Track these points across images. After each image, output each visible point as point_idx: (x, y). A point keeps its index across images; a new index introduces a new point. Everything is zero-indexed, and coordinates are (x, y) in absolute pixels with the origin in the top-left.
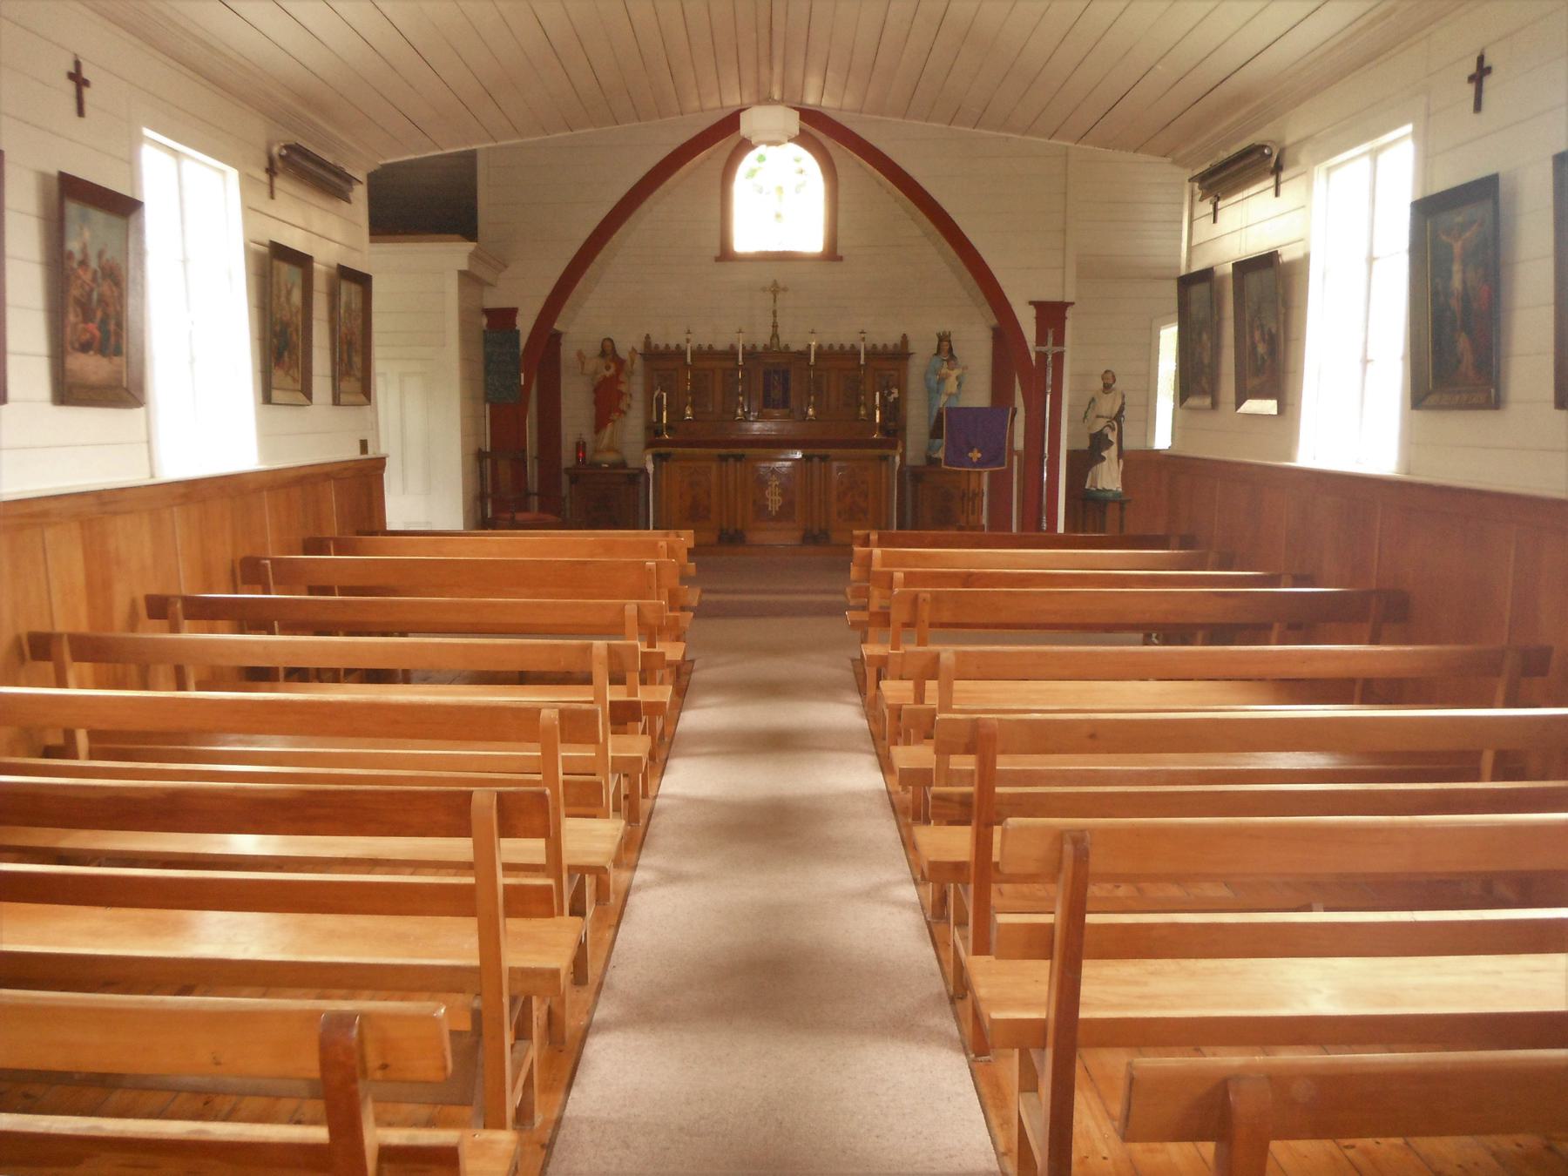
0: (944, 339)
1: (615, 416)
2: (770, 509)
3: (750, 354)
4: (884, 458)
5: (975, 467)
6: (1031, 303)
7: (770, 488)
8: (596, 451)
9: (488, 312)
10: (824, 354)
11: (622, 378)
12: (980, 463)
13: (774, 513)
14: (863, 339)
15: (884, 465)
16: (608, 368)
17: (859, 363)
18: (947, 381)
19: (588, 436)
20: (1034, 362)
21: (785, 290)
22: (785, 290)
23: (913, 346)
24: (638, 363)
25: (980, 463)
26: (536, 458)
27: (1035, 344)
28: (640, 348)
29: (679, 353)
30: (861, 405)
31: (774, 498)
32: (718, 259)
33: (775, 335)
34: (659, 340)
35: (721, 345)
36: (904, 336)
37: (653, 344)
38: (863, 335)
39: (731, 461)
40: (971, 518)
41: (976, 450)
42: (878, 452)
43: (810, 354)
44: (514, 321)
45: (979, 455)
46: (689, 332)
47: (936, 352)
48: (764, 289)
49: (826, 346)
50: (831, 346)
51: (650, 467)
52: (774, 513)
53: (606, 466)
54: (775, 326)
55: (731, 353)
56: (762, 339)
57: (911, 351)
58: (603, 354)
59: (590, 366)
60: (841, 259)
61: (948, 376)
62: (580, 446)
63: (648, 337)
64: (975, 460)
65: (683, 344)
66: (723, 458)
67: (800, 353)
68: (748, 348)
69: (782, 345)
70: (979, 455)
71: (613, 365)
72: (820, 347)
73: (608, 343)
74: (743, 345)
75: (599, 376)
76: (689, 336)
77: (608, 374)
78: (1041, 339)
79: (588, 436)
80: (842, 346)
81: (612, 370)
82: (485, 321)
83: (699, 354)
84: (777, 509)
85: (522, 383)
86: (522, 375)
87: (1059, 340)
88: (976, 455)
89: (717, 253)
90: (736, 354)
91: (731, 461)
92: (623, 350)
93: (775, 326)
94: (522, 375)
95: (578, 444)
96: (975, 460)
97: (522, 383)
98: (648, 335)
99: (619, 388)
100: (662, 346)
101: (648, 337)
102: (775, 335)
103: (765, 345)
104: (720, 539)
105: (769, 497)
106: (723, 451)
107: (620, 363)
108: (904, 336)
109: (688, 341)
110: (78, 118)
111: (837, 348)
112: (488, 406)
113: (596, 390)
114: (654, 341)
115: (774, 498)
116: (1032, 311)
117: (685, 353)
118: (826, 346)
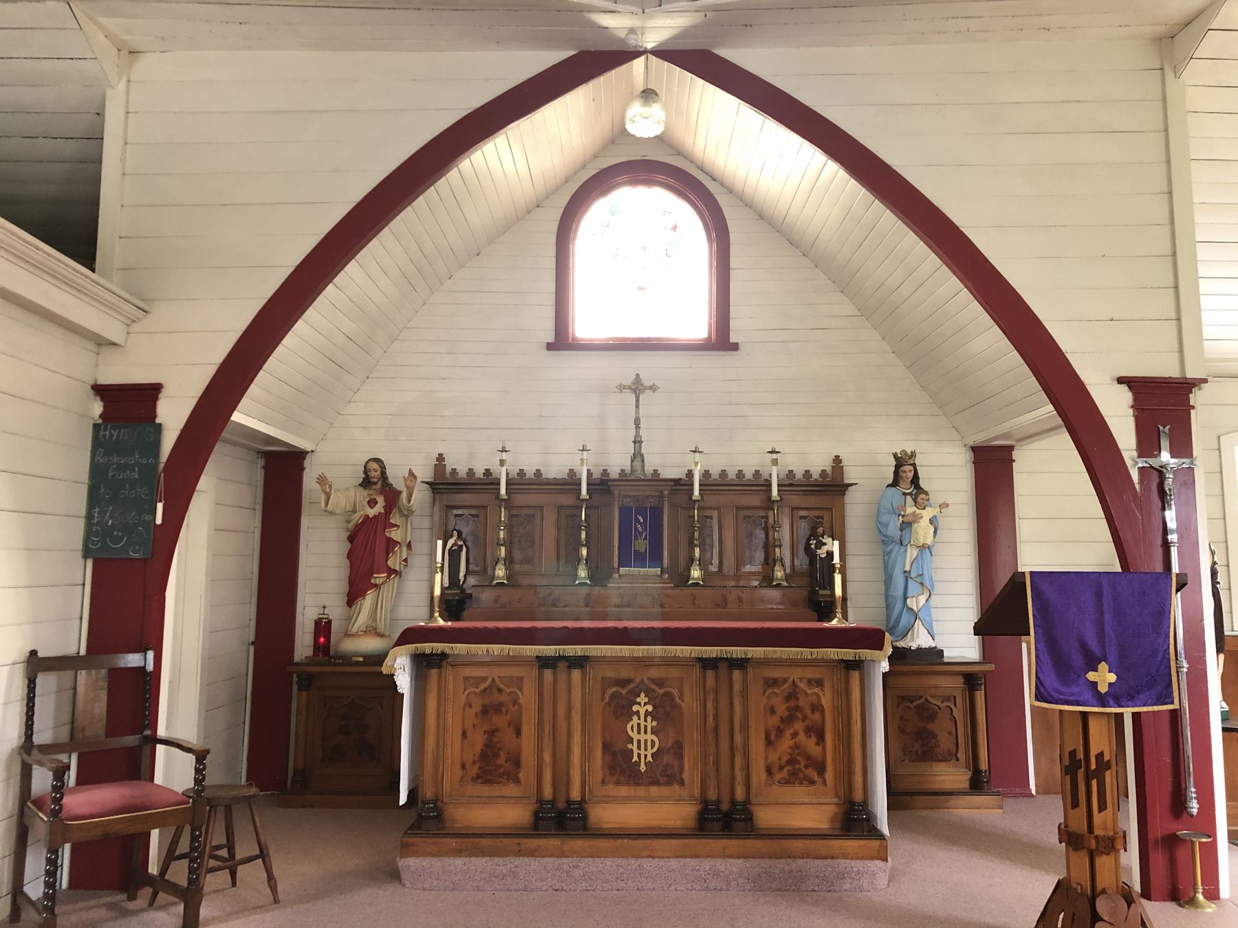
0: (901, 461)
1: (379, 578)
2: (635, 758)
3: (602, 485)
4: (856, 665)
5: (1103, 704)
6: (1121, 380)
7: (635, 718)
8: (347, 635)
9: (101, 390)
10: (715, 485)
11: (395, 518)
12: (1116, 695)
13: (643, 768)
14: (775, 462)
15: (855, 675)
16: (372, 503)
17: (770, 497)
18: (915, 526)
19: (336, 612)
20: (1137, 486)
21: (653, 388)
22: (653, 388)
23: (850, 475)
24: (421, 496)
25: (1116, 695)
26: (253, 643)
27: (1135, 454)
28: (425, 472)
29: (489, 481)
30: (774, 562)
31: (642, 737)
32: (550, 347)
33: (638, 456)
34: (459, 462)
35: (555, 469)
36: (837, 460)
37: (448, 470)
38: (774, 456)
39: (562, 665)
40: (1097, 818)
41: (1103, 666)
42: (848, 654)
43: (692, 485)
44: (154, 407)
45: (1112, 678)
46: (503, 450)
47: (890, 481)
48: (621, 388)
49: (715, 473)
50: (723, 473)
51: (404, 682)
52: (643, 768)
53: (361, 659)
54: (637, 442)
55: (572, 482)
56: (618, 461)
57: (846, 481)
58: (366, 483)
59: (340, 501)
60: (735, 347)
61: (916, 518)
62: (323, 627)
63: (441, 458)
64: (1103, 689)
65: (494, 465)
66: (545, 663)
67: (677, 482)
68: (597, 475)
69: (649, 470)
70: (1112, 678)
71: (381, 500)
72: (706, 474)
73: (375, 466)
74: (589, 471)
75: (357, 515)
76: (505, 456)
77: (372, 512)
78: (1147, 445)
79: (336, 612)
80: (740, 474)
81: (379, 508)
82: (97, 408)
83: (518, 483)
84: (649, 758)
85: (159, 521)
86: (160, 506)
87: (1182, 447)
88: (1104, 677)
89: (551, 338)
90: (578, 484)
91: (562, 665)
92: (396, 477)
93: (637, 442)
94: (160, 506)
95: (318, 623)
96: (1103, 689)
97: (159, 521)
98: (440, 455)
99: (388, 534)
100: (462, 471)
101: (441, 458)
102: (638, 456)
103: (623, 471)
104: (537, 816)
105: (634, 735)
106: (550, 650)
107: (392, 497)
108: (837, 460)
109: (502, 463)
110: (164, 385)
111: (732, 474)
112: (90, 564)
113: (351, 539)
114: (450, 464)
115: (642, 737)
116: (1125, 396)
117: (497, 483)
118: (715, 473)
